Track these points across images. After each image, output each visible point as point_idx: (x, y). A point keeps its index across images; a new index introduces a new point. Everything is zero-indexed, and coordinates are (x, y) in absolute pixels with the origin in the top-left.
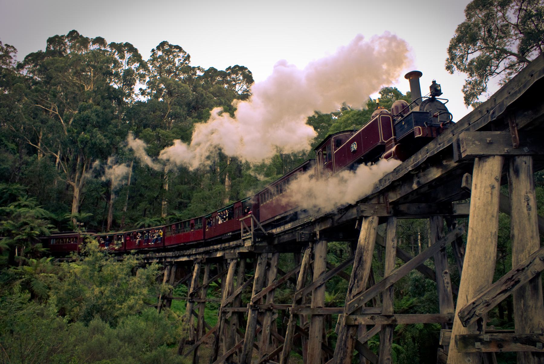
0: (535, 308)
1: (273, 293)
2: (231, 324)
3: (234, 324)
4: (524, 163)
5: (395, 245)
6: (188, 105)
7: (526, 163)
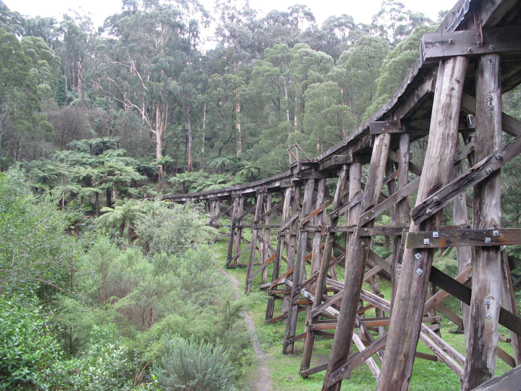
0: (490, 206)
1: (320, 215)
2: (290, 246)
3: (293, 247)
4: (489, 62)
5: (407, 161)
6: (251, 46)
7: (491, 62)
